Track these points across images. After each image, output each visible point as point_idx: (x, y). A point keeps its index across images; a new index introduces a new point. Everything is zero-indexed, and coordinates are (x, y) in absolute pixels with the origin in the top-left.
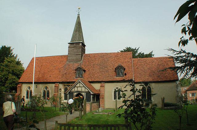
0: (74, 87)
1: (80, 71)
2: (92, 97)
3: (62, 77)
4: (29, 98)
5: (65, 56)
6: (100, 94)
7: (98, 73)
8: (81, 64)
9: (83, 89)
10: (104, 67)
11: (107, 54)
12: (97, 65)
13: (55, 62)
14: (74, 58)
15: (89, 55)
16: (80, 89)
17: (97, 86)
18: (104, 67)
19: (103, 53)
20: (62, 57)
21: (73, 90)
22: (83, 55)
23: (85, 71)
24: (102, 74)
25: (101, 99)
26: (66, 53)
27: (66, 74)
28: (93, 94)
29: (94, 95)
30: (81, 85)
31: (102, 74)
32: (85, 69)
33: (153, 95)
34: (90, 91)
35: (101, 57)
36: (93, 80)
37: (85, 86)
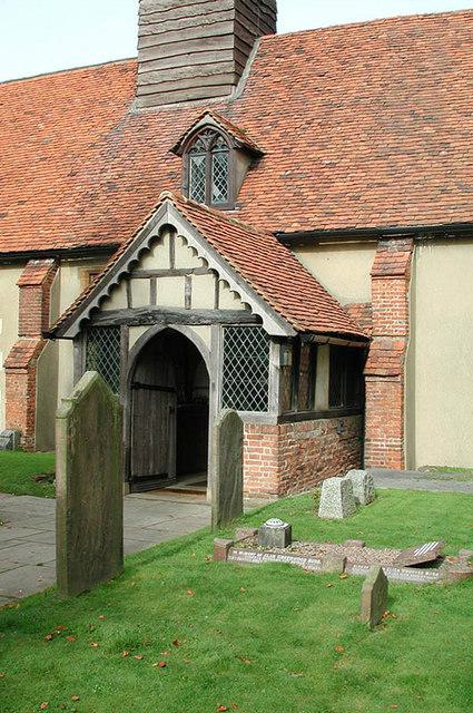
0: (126, 277)
1: (219, 155)
2: (274, 361)
3: (82, 211)
4: (274, 399)
5: (125, 68)
6: (368, 340)
7: (359, 164)
8: (240, 107)
9: (203, 295)
10: (412, 113)
11: (345, 29)
12: (355, 104)
13: (54, 115)
14: (185, 65)
15: (300, 40)
16: (170, 295)
17: (345, 276)
18: (412, 113)
19: (406, 20)
20: (101, 71)
21: (119, 302)
22: (257, 46)
23: (252, 155)
24: (393, 170)
25: (375, 389)
26: (121, 43)
27: (111, 186)
28: (282, 332)
29: (300, 347)
30: (184, 259)
31: (393, 170)
32: (262, 145)
33: (189, 298)
34: (257, 309)
35: (392, 44)
36: (315, 221)
37: (214, 264)
